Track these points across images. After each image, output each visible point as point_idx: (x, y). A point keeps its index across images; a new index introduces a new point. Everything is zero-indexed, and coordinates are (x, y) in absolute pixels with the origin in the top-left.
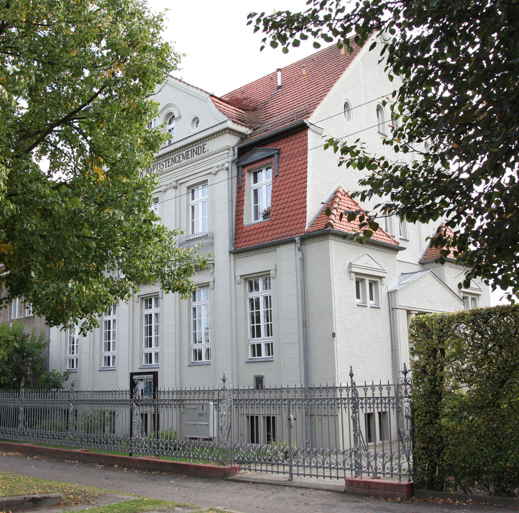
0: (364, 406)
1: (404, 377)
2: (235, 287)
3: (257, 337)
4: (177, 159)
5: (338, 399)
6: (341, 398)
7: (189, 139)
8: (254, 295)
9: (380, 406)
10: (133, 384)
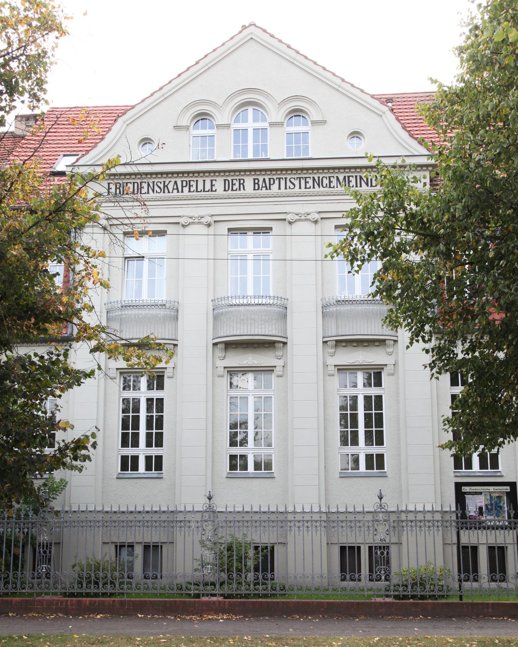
0: (414, 529)
1: (379, 502)
2: (324, 381)
3: (156, 446)
4: (326, 182)
5: (403, 521)
6: (407, 521)
7: (359, 160)
8: (130, 394)
9: (319, 528)
10: (460, 498)
